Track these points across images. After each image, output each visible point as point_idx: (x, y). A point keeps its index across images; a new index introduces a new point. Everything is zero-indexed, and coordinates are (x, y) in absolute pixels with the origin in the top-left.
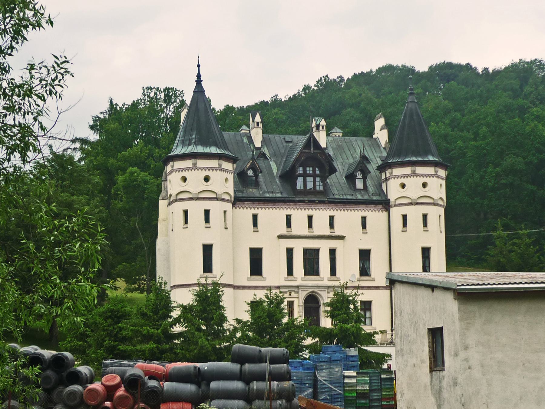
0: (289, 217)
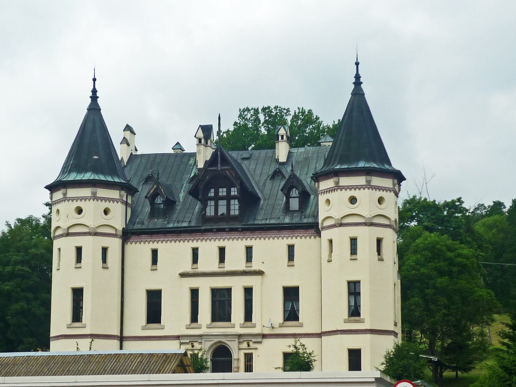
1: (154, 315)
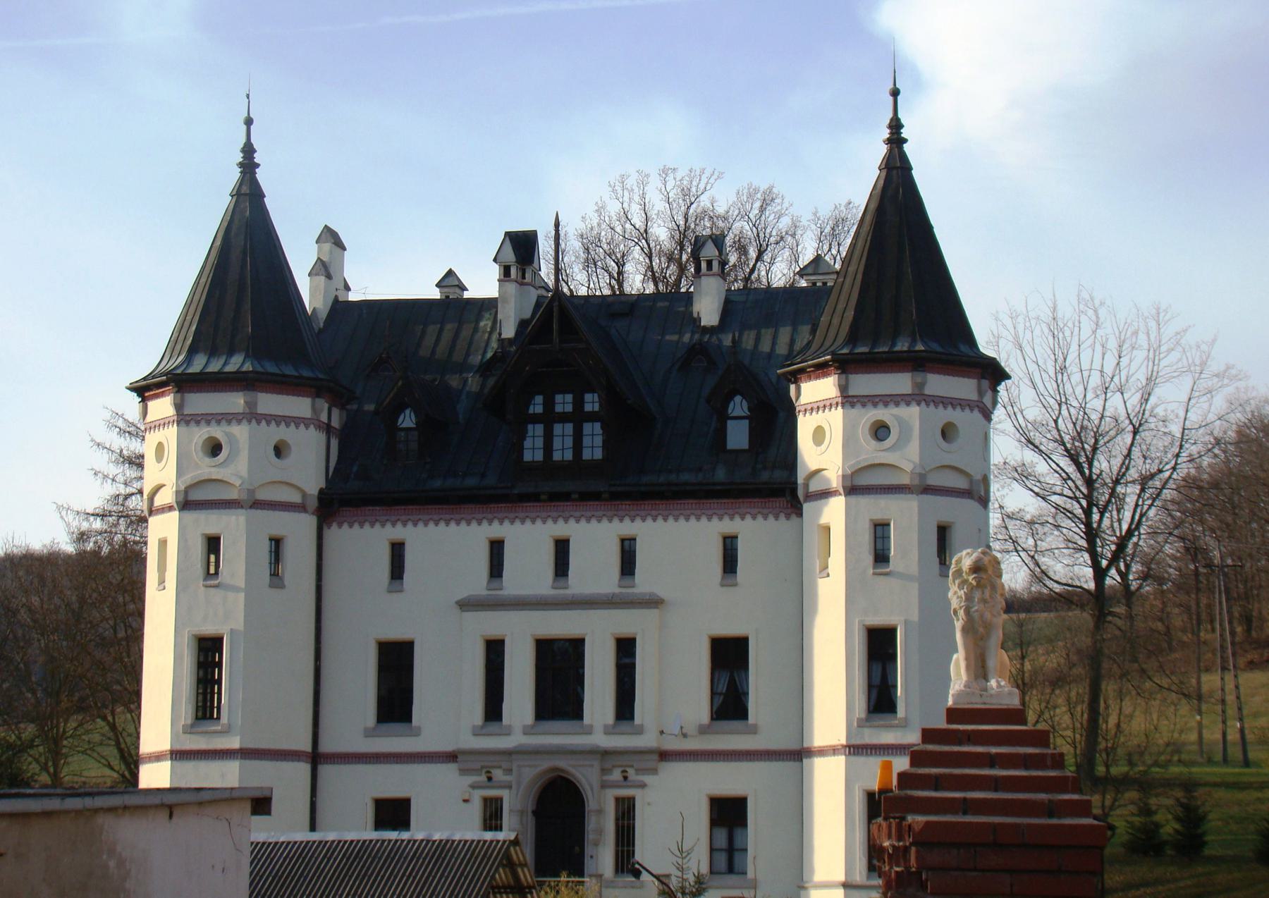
0: (728, 541)
1: (395, 703)
